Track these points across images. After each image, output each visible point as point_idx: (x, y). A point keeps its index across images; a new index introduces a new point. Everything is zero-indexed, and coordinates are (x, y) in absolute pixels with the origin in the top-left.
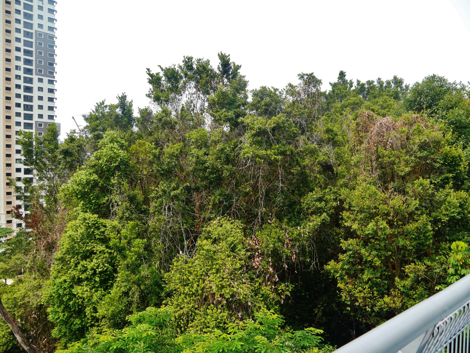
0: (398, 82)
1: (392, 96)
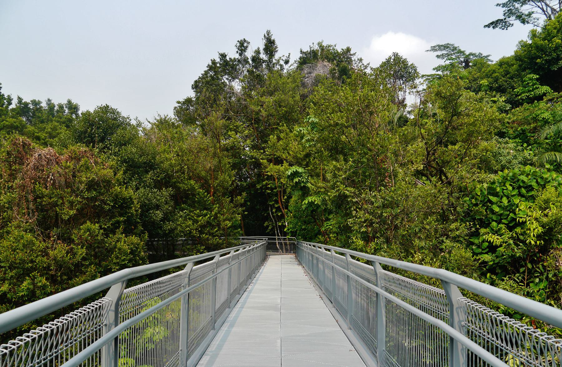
0: (73, 108)
1: (64, 123)
